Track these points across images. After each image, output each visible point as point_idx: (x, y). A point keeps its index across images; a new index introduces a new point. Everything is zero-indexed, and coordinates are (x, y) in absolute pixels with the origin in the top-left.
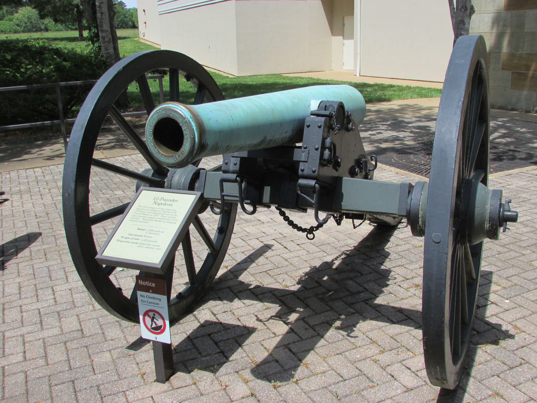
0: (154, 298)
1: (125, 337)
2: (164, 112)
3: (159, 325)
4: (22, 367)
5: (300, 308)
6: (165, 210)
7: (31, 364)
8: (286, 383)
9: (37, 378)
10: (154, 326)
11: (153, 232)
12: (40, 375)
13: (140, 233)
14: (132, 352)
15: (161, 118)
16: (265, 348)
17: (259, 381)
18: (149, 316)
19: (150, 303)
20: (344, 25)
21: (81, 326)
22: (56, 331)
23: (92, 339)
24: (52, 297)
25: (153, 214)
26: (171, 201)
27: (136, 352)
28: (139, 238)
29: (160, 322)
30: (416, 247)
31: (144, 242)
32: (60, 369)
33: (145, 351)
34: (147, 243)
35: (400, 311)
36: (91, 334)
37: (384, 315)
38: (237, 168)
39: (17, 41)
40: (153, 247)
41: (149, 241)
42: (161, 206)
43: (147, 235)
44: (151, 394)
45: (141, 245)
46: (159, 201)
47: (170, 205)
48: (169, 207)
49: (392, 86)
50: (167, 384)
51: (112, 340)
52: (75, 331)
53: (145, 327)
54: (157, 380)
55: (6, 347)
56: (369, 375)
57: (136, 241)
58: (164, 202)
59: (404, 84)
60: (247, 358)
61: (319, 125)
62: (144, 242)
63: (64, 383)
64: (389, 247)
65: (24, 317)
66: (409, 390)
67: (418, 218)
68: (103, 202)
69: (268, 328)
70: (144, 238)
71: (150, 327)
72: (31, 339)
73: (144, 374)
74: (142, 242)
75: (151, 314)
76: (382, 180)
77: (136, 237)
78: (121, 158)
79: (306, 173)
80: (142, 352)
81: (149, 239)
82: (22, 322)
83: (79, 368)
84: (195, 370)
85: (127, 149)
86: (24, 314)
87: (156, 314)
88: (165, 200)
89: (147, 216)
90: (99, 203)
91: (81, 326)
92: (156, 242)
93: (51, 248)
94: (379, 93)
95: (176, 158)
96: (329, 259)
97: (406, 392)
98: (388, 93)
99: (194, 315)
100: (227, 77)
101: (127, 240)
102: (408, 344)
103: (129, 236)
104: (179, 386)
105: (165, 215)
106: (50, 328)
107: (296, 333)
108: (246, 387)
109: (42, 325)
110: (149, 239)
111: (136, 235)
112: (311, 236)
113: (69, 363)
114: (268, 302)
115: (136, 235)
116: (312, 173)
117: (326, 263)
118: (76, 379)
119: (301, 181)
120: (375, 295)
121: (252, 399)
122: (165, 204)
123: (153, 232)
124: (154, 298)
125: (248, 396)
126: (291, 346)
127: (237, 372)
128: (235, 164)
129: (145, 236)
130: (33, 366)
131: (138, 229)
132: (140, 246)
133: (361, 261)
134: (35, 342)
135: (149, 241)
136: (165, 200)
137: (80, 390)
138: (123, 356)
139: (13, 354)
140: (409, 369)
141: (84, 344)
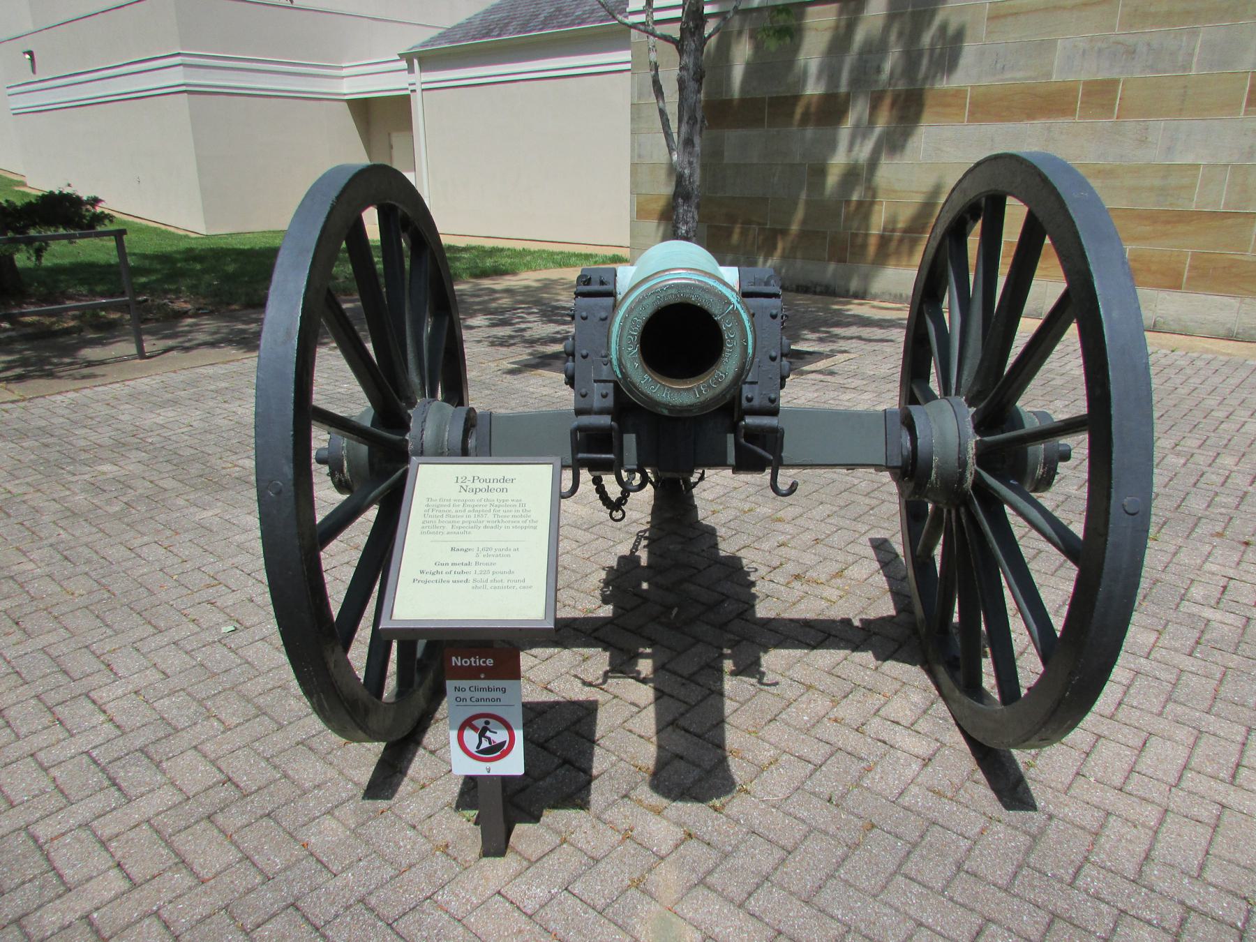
0: (489, 689)
1: (341, 773)
2: (674, 291)
3: (498, 741)
4: (140, 904)
7: (159, 891)
8: (729, 797)
9: (198, 921)
10: (485, 744)
11: (492, 553)
12: (200, 911)
14: (382, 804)
15: (663, 305)
17: (680, 804)
18: (475, 729)
19: (478, 700)
20: (391, 147)
21: (219, 769)
22: (167, 796)
23: (271, 795)
24: (102, 718)
25: (472, 514)
27: (391, 802)
28: (465, 569)
29: (500, 736)
31: (484, 577)
32: (241, 884)
33: (410, 795)
34: (490, 577)
35: (806, 624)
36: (259, 784)
37: (787, 637)
38: (609, 402)
39: (851, 71)
42: (480, 495)
43: (481, 559)
44: (493, 887)
45: (479, 585)
46: (471, 486)
48: (503, 496)
49: (502, 250)
50: (510, 856)
51: (318, 786)
52: (215, 784)
53: (461, 752)
54: (486, 853)
55: (58, 864)
56: (850, 749)
57: (463, 577)
58: (484, 485)
59: (519, 246)
60: (622, 764)
61: (774, 312)
62: (484, 577)
63: (274, 915)
64: (705, 514)
65: (59, 781)
66: (927, 762)
67: (931, 468)
68: (83, 490)
69: (615, 697)
70: (479, 568)
71: (473, 749)
72: (117, 830)
73: (447, 846)
74: (478, 577)
75: (480, 723)
76: (827, 406)
77: (459, 569)
78: (59, 398)
79: (756, 403)
80: (402, 799)
81: (492, 568)
82: (62, 792)
83: (285, 870)
84: (545, 812)
85: (60, 378)
86: (55, 772)
87: (491, 721)
90: (74, 494)
91: (219, 769)
93: (20, 605)
94: (489, 262)
95: (700, 392)
96: (625, 549)
97: (925, 765)
98: (505, 261)
100: (186, 236)
101: (438, 577)
102: (863, 680)
103: (440, 568)
104: (539, 853)
105: (501, 513)
106: (150, 791)
107: (672, 697)
108: (665, 822)
109: (120, 789)
110: (492, 568)
112: (618, 515)
113: (254, 864)
114: (578, 646)
116: (769, 404)
117: (622, 559)
118: (297, 899)
119: (750, 420)
121: (693, 843)
122: (488, 490)
123: (492, 553)
124: (489, 689)
125: (683, 841)
126: (682, 722)
127: (625, 796)
128: (604, 396)
130: (166, 895)
133: (679, 547)
134: (132, 834)
137: (327, 922)
138: (369, 818)
139: (91, 878)
140: (898, 723)
141: (260, 812)
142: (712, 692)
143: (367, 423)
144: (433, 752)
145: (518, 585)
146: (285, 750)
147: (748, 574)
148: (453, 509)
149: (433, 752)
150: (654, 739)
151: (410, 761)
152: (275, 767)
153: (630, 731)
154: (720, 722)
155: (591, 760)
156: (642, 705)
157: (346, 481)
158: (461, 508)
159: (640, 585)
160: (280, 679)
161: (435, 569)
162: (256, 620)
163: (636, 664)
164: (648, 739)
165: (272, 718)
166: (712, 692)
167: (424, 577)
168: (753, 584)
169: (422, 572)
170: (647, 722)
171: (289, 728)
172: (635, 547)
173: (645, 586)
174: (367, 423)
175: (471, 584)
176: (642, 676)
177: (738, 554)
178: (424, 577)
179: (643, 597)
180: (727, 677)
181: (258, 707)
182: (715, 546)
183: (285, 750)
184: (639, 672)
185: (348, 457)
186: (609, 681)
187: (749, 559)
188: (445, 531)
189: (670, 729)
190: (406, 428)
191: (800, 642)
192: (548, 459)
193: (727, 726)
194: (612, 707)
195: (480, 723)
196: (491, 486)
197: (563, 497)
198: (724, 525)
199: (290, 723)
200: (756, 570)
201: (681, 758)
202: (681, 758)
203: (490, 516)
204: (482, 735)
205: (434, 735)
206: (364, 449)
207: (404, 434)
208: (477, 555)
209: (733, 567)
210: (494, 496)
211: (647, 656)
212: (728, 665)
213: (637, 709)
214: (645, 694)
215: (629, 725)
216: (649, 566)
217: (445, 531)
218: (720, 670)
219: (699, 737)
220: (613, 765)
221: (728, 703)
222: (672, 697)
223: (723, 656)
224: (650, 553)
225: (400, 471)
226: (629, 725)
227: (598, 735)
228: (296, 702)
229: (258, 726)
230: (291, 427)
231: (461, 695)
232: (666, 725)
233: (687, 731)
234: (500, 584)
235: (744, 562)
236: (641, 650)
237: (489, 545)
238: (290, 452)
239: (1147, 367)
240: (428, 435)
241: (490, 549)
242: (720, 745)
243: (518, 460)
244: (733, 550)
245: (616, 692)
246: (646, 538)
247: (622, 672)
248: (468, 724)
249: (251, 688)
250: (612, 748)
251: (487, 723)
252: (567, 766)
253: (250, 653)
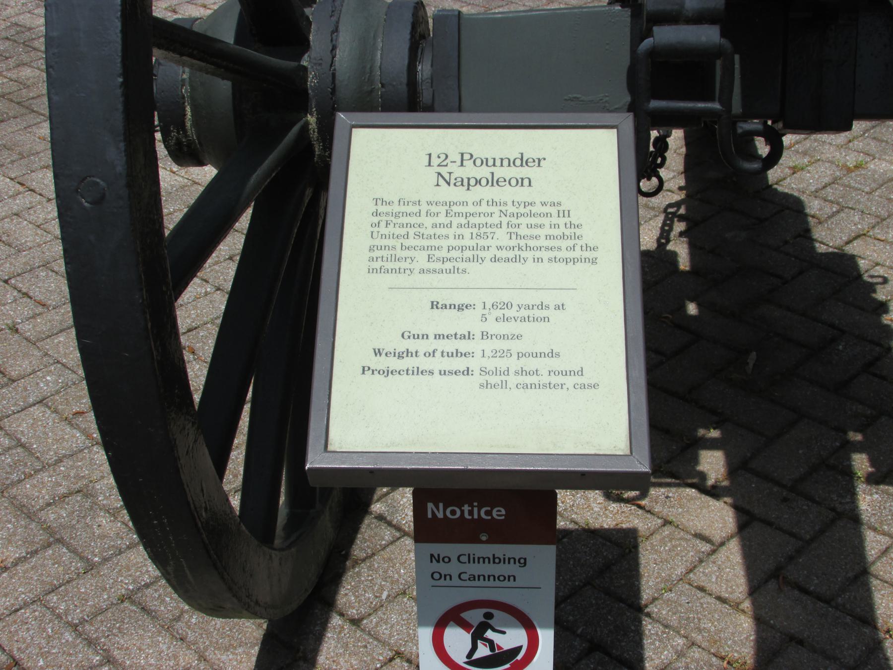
0: (495, 560)
1: (202, 658)
5: (707, 428)
6: (511, 209)
10: (483, 651)
13: (448, 322)
16: (723, 600)
18: (465, 625)
19: (473, 578)
25: (466, 232)
26: (511, 163)
28: (463, 346)
30: (850, 170)
31: (502, 364)
40: (555, 380)
41: (520, 355)
42: (479, 192)
45: (493, 380)
46: (459, 172)
47: (520, 182)
48: (522, 194)
57: (459, 364)
60: (696, 653)
62: (502, 364)
69: (667, 522)
70: (489, 345)
71: (460, 658)
74: (491, 364)
75: (475, 616)
77: (449, 346)
81: (515, 346)
88: (485, 162)
89: (444, 243)
99: (381, 518)
103: (412, 345)
107: (769, 524)
110: (515, 346)
111: (438, 337)
115: (438, 337)
120: (879, 345)
122: (493, 182)
124: (495, 560)
129: (485, 335)
131: (434, 305)
132: (486, 385)
135: (520, 355)
136: (485, 162)
142: (839, 515)
143: (227, 35)
144: (356, 622)
145: (570, 381)
146: (102, 611)
147: (871, 288)
148: (428, 221)
149: (356, 622)
150: (747, 605)
151: (319, 638)
152: (91, 642)
153: (702, 589)
154: (861, 574)
155: (639, 645)
156: (717, 539)
157: (190, 144)
158: (442, 219)
159: (683, 308)
160: (78, 477)
161: (402, 346)
162: (25, 365)
163: (696, 460)
164: (736, 606)
165: (74, 551)
166: (839, 515)
167: (382, 363)
168: (883, 307)
169: (378, 352)
170: (730, 571)
171: (104, 570)
172: (665, 235)
173: (692, 309)
174: (227, 35)
175: (478, 378)
176: (710, 482)
177: (850, 249)
178: (382, 363)
179: (684, 324)
180: (861, 487)
181: (48, 530)
182: (806, 234)
183: (102, 611)
184: (703, 476)
185: (192, 98)
186: (653, 491)
187: (870, 257)
188: (416, 266)
189: (772, 585)
190: (304, 45)
192: (609, 118)
193: (875, 582)
194: (663, 542)
195: (475, 616)
196: (499, 172)
198: (815, 194)
199: (105, 560)
200: (885, 281)
201: (801, 642)
202: (801, 642)
203: (501, 237)
204: (478, 635)
205: (355, 589)
206: (224, 87)
207: (299, 57)
208: (484, 318)
209: (842, 270)
210: (506, 194)
211: (712, 445)
212: (861, 463)
213: (706, 547)
214: (719, 517)
215: (698, 577)
216: (695, 271)
217: (416, 266)
218: (849, 474)
219: (827, 602)
220: (680, 654)
221: (870, 537)
222: (769, 524)
223: (850, 447)
224: (693, 248)
225: (296, 129)
226: (698, 577)
227: (645, 596)
228: (110, 523)
229: (55, 564)
230: (118, 67)
231: (443, 568)
232: (764, 579)
233: (804, 591)
234: (534, 379)
235: (862, 264)
236: (701, 432)
238: (118, 118)
240: (344, 58)
241: (508, 305)
242: (866, 618)
243: (545, 118)
244: (839, 242)
245: (672, 513)
246: (681, 218)
247: (672, 476)
248: (453, 617)
249: (37, 490)
250: (674, 620)
251: (489, 616)
252: (598, 655)
253: (22, 426)
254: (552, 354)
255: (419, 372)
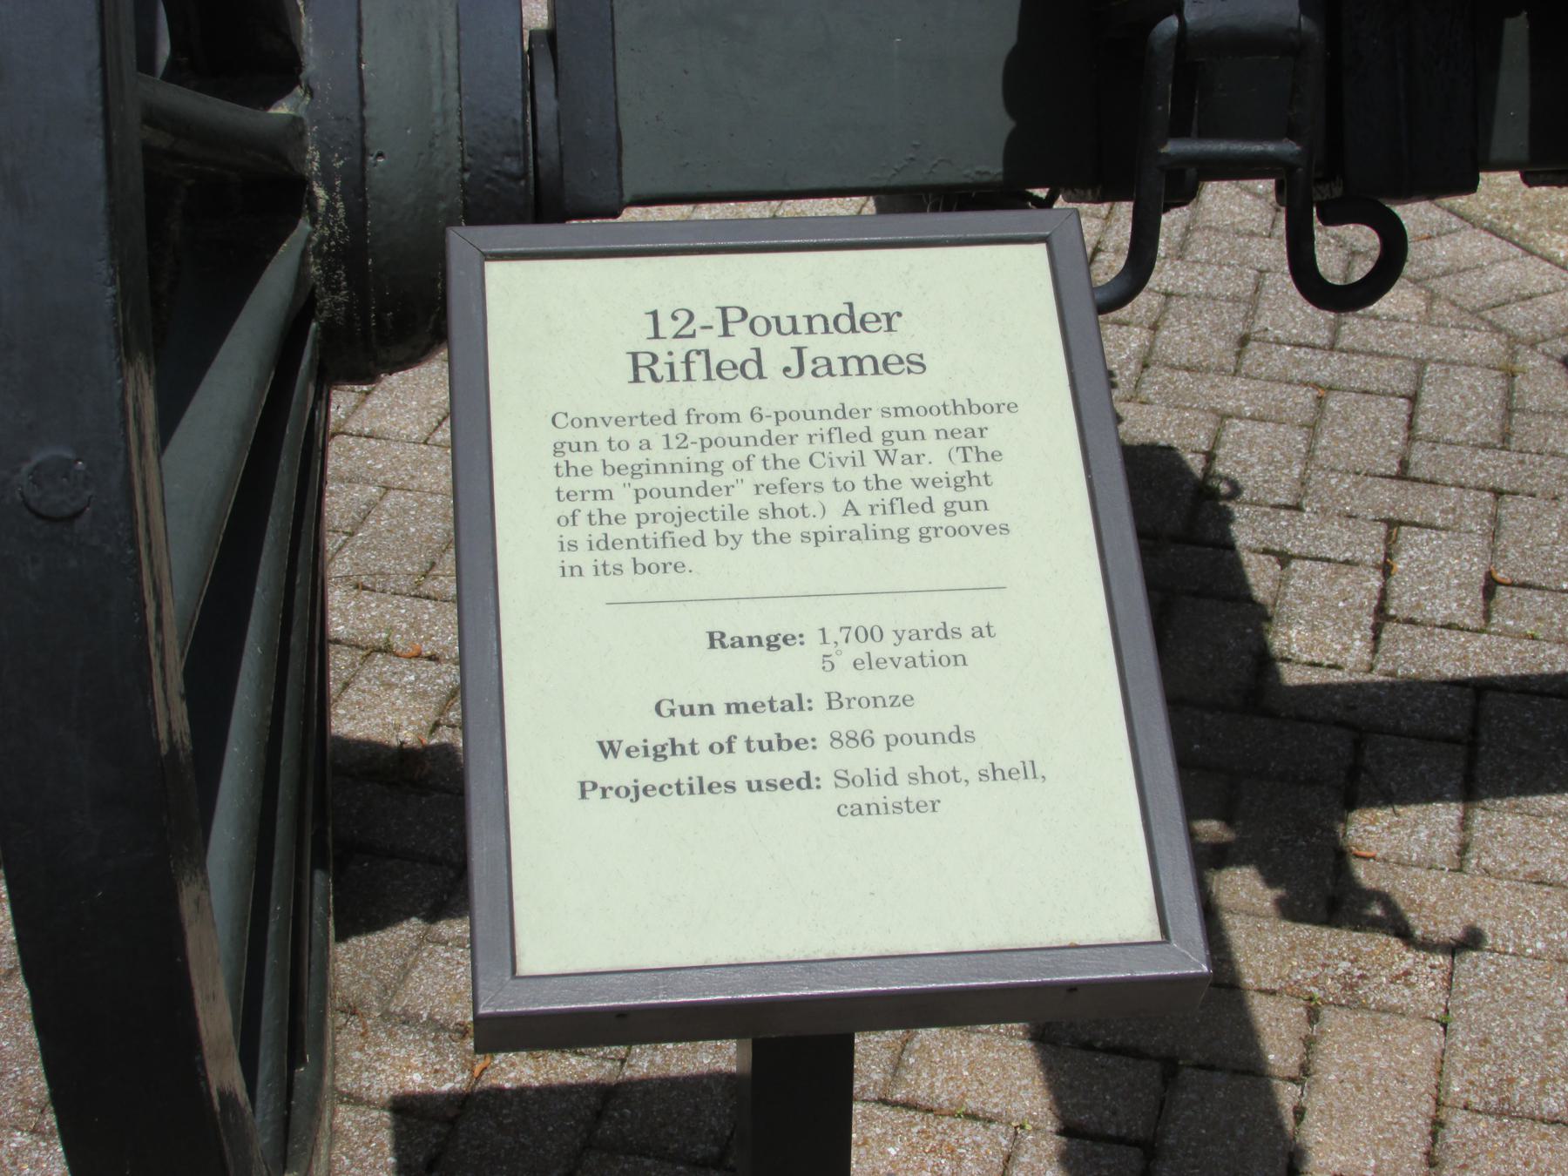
26: (831, 325)
28: (792, 725)
43: (850, 683)
77: (762, 726)
81: (882, 722)
92: (959, 736)
101: (677, 768)
103: (683, 729)
110: (882, 722)
161: (660, 731)
167: (620, 771)
169: (608, 749)
178: (620, 771)
191: (1541, 694)
196: (819, 345)
197: (1103, 308)
210: (735, 395)
237: (863, 614)
239: (1338, 926)
254: (959, 736)
255: (703, 787)
